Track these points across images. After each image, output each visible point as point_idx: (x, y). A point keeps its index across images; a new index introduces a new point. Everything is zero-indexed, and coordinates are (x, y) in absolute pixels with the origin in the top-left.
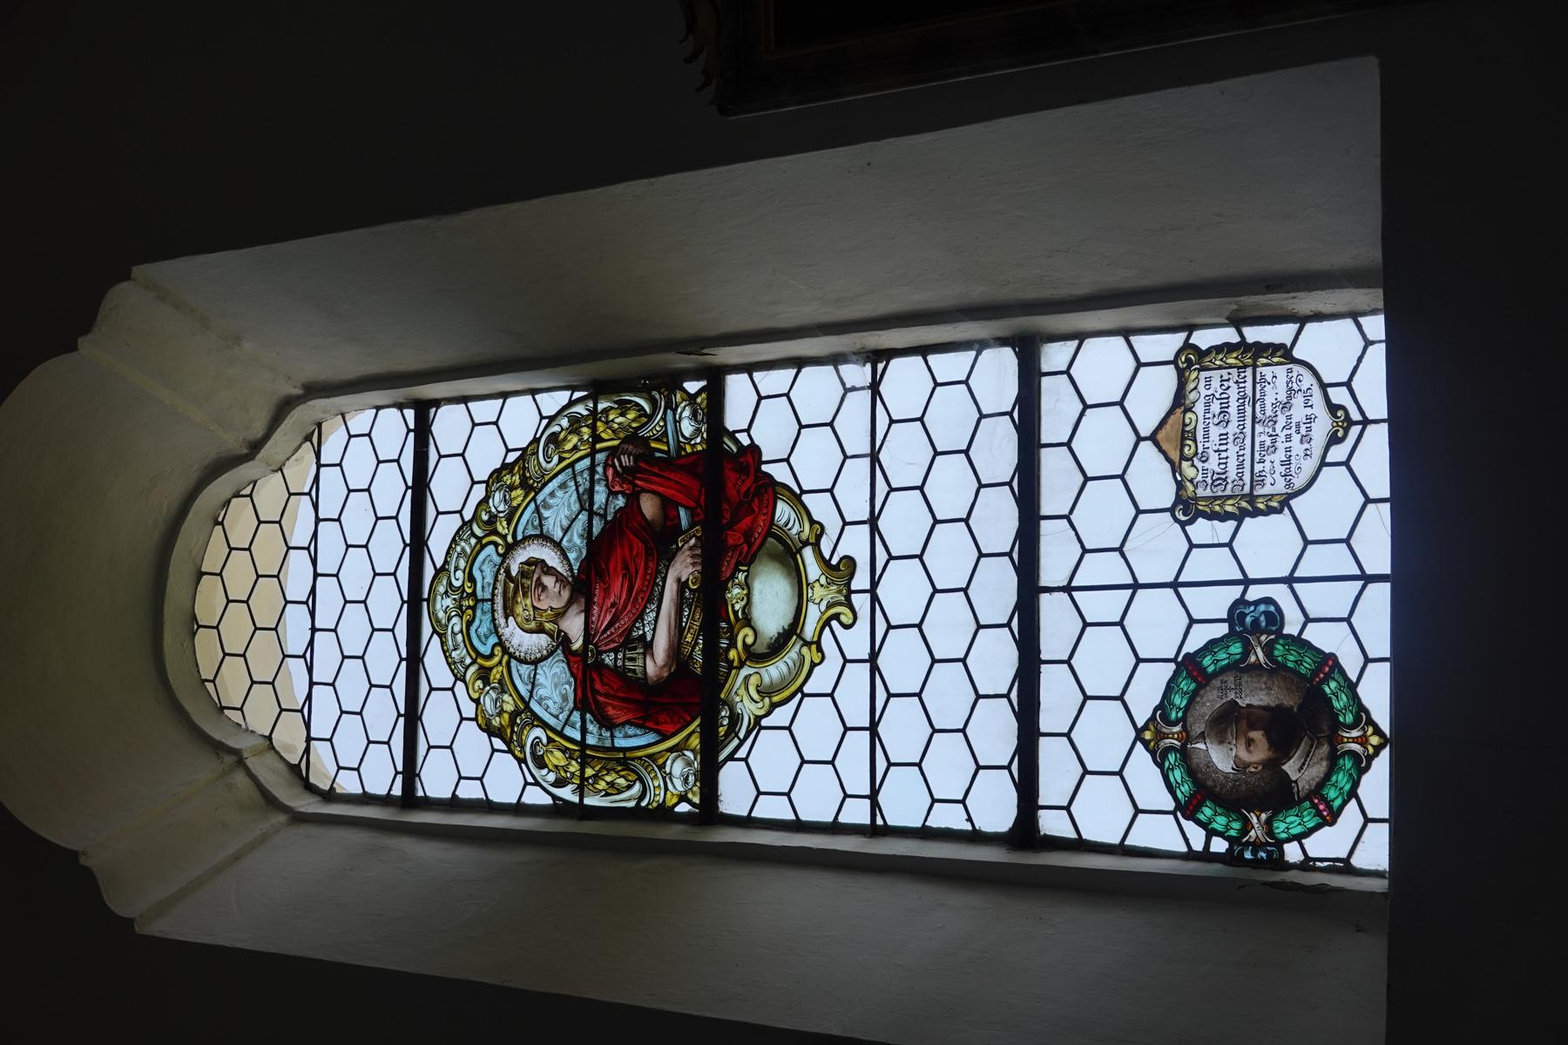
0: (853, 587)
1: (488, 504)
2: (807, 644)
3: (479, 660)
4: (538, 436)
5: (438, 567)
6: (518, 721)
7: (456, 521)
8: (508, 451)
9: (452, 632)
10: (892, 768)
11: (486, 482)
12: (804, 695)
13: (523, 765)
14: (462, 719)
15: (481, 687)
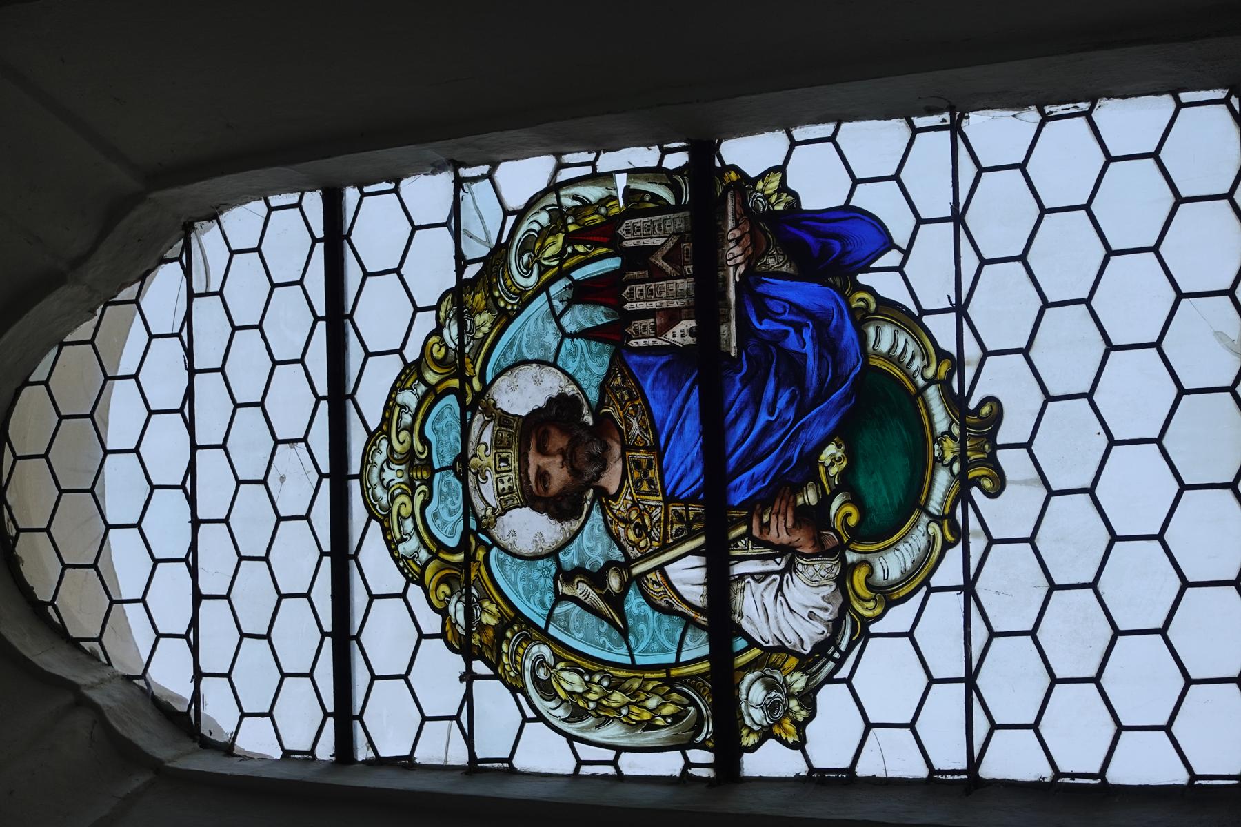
4: (504, 240)
6: (509, 634)
7: (394, 366)
9: (399, 514)
11: (437, 308)
12: (931, 590)
14: (421, 636)
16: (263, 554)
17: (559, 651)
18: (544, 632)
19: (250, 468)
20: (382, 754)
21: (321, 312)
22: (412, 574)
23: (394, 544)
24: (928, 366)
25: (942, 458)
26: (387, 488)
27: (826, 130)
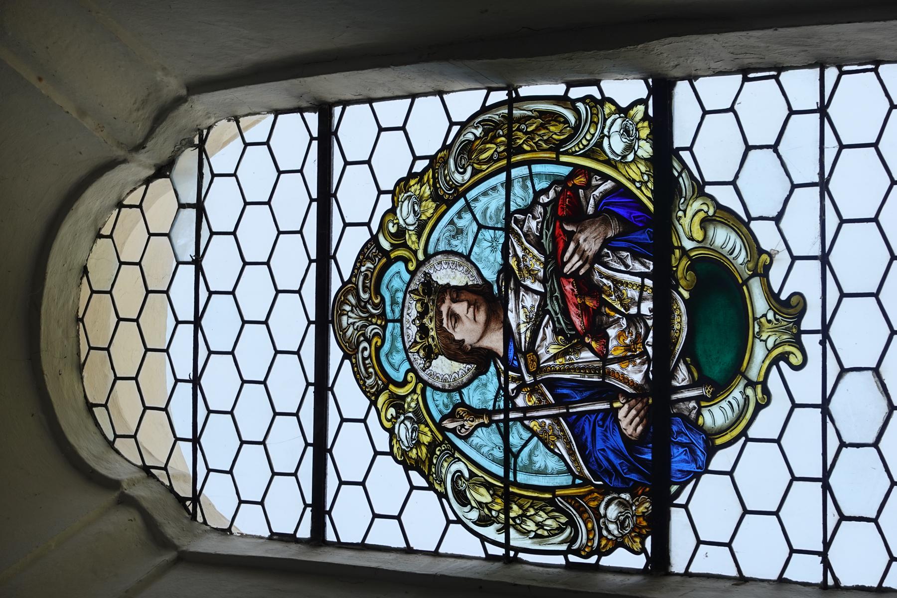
0: (803, 328)
1: (396, 214)
2: (751, 384)
3: (391, 387)
4: (449, 142)
5: (345, 280)
8: (416, 158)
10: (845, 226)
11: (392, 192)
13: (444, 501)
14: (377, 453)
15: (394, 414)
16: (262, 379)
17: (480, 175)
20: (342, 540)
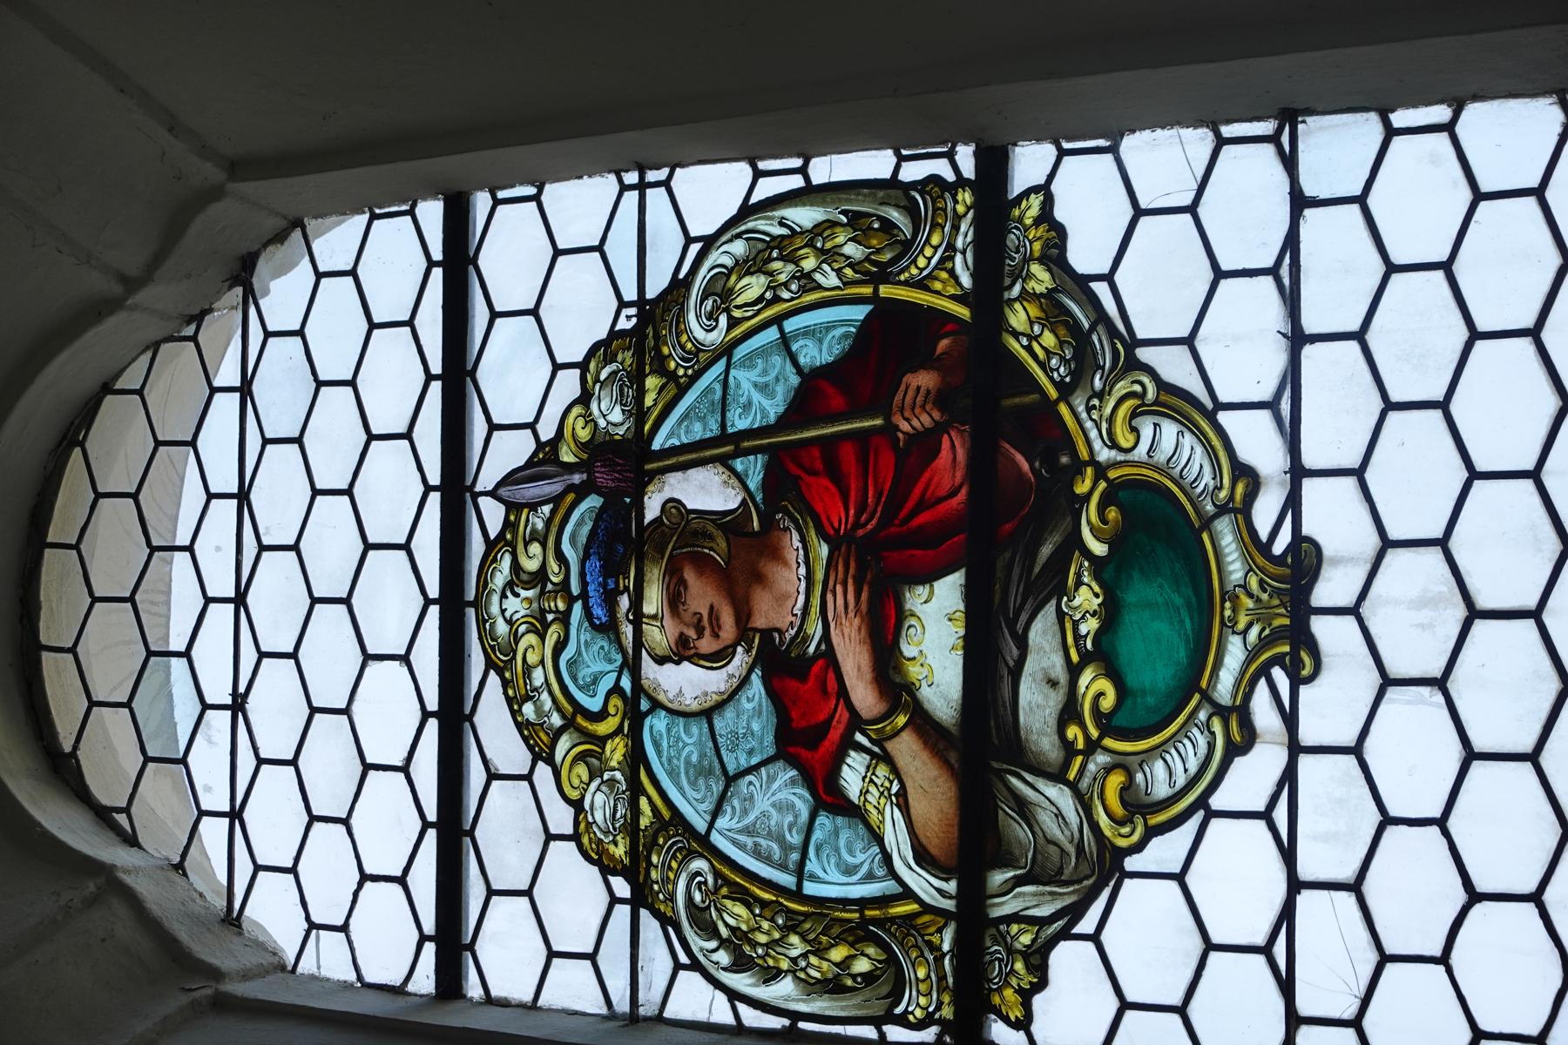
4: (681, 276)
5: (492, 536)
11: (583, 366)
12: (1211, 814)
18: (704, 840)
19: (330, 579)
21: (436, 369)
22: (539, 746)
23: (518, 703)
24: (1220, 488)
25: (1234, 621)
26: (510, 622)
27: (1440, 113)
